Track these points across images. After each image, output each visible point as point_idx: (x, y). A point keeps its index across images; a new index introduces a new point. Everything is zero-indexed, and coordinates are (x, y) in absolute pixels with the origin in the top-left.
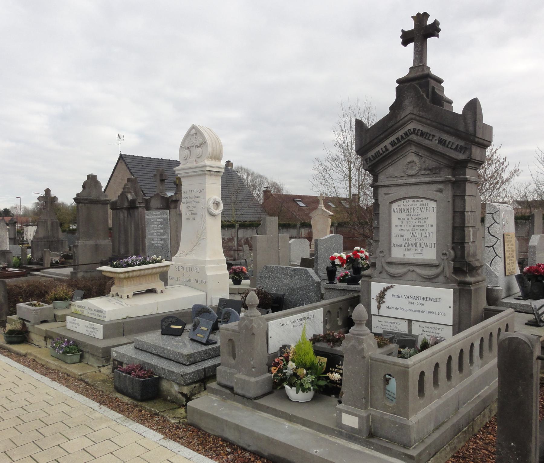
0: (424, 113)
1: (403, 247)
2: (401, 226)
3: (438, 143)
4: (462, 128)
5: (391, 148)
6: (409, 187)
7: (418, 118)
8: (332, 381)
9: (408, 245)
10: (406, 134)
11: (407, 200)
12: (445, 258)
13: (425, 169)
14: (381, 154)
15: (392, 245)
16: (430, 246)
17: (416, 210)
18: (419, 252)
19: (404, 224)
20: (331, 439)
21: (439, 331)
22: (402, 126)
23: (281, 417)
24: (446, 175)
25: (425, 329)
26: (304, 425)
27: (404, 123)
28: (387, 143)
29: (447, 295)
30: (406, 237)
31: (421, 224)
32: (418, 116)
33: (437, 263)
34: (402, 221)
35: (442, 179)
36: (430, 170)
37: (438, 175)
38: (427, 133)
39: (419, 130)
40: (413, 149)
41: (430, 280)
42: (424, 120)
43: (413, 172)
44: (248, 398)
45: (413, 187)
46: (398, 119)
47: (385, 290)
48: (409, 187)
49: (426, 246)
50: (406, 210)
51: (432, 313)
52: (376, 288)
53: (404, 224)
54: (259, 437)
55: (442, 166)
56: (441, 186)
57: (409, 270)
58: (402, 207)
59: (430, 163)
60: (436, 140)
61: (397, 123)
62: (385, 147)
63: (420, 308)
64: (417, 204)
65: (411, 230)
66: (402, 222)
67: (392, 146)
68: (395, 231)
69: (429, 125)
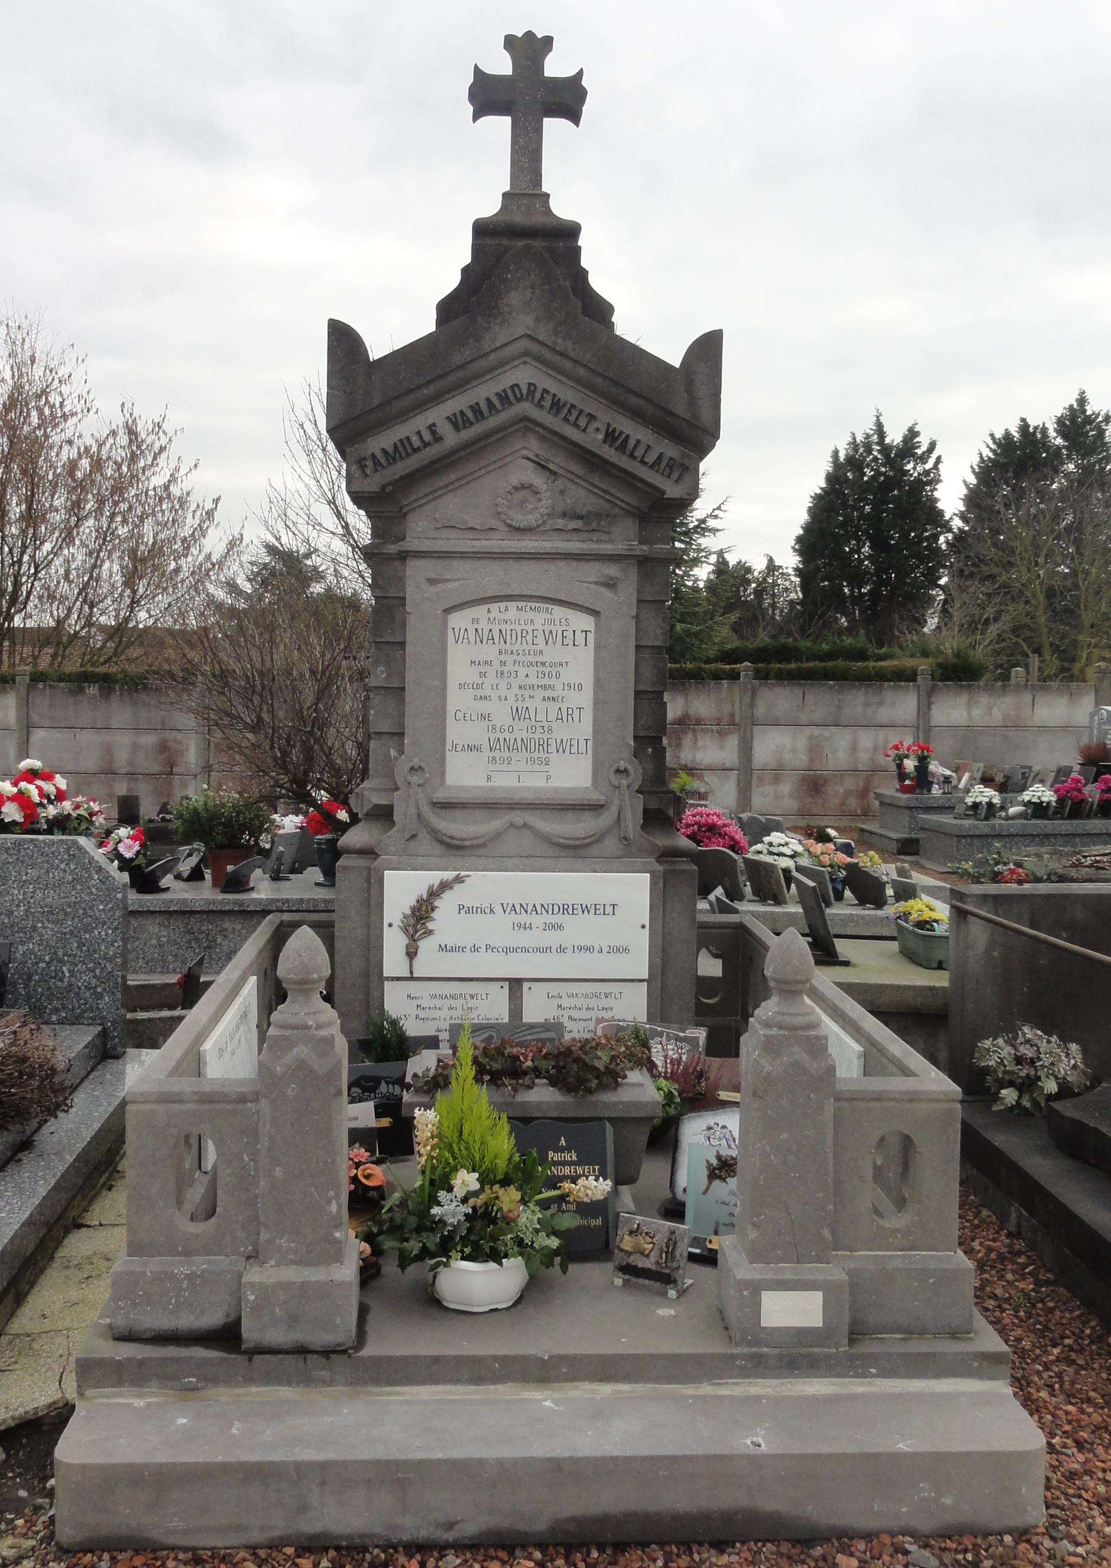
0: (569, 344)
1: (486, 753)
2: (480, 686)
3: (604, 441)
4: (680, 407)
5: (451, 438)
6: (513, 565)
7: (548, 355)
8: (586, 1209)
9: (502, 747)
10: (503, 397)
11: (503, 605)
12: (624, 782)
13: (564, 515)
14: (416, 450)
15: (449, 746)
16: (574, 749)
17: (529, 638)
18: (537, 768)
19: (492, 678)
20: (724, 1391)
21: (609, 1002)
22: (490, 370)
23: (497, 1380)
24: (622, 538)
25: (566, 1002)
26: (605, 1377)
27: (502, 364)
28: (438, 414)
29: (631, 891)
30: (497, 721)
31: (547, 681)
32: (553, 350)
33: (596, 797)
34: (483, 669)
35: (619, 548)
36: (581, 517)
37: (603, 536)
38: (573, 406)
39: (545, 391)
40: (533, 446)
41: (575, 853)
42: (568, 365)
43: (531, 520)
44: (327, 1353)
45: (527, 566)
46: (486, 345)
47: (434, 893)
48: (511, 563)
49: (561, 748)
50: (496, 635)
51: (589, 949)
52: (401, 888)
53: (492, 678)
54: (508, 1473)
55: (616, 511)
56: (612, 570)
57: (511, 824)
58: (484, 625)
59: (581, 497)
60: (597, 430)
61: (480, 357)
62: (432, 428)
63: (554, 938)
64: (539, 618)
65: (511, 698)
66: (483, 675)
67: (457, 428)
68: (457, 700)
69: (578, 380)
